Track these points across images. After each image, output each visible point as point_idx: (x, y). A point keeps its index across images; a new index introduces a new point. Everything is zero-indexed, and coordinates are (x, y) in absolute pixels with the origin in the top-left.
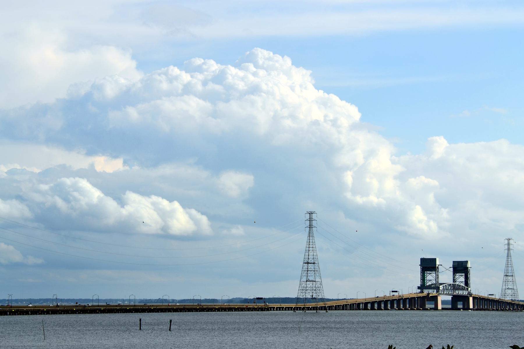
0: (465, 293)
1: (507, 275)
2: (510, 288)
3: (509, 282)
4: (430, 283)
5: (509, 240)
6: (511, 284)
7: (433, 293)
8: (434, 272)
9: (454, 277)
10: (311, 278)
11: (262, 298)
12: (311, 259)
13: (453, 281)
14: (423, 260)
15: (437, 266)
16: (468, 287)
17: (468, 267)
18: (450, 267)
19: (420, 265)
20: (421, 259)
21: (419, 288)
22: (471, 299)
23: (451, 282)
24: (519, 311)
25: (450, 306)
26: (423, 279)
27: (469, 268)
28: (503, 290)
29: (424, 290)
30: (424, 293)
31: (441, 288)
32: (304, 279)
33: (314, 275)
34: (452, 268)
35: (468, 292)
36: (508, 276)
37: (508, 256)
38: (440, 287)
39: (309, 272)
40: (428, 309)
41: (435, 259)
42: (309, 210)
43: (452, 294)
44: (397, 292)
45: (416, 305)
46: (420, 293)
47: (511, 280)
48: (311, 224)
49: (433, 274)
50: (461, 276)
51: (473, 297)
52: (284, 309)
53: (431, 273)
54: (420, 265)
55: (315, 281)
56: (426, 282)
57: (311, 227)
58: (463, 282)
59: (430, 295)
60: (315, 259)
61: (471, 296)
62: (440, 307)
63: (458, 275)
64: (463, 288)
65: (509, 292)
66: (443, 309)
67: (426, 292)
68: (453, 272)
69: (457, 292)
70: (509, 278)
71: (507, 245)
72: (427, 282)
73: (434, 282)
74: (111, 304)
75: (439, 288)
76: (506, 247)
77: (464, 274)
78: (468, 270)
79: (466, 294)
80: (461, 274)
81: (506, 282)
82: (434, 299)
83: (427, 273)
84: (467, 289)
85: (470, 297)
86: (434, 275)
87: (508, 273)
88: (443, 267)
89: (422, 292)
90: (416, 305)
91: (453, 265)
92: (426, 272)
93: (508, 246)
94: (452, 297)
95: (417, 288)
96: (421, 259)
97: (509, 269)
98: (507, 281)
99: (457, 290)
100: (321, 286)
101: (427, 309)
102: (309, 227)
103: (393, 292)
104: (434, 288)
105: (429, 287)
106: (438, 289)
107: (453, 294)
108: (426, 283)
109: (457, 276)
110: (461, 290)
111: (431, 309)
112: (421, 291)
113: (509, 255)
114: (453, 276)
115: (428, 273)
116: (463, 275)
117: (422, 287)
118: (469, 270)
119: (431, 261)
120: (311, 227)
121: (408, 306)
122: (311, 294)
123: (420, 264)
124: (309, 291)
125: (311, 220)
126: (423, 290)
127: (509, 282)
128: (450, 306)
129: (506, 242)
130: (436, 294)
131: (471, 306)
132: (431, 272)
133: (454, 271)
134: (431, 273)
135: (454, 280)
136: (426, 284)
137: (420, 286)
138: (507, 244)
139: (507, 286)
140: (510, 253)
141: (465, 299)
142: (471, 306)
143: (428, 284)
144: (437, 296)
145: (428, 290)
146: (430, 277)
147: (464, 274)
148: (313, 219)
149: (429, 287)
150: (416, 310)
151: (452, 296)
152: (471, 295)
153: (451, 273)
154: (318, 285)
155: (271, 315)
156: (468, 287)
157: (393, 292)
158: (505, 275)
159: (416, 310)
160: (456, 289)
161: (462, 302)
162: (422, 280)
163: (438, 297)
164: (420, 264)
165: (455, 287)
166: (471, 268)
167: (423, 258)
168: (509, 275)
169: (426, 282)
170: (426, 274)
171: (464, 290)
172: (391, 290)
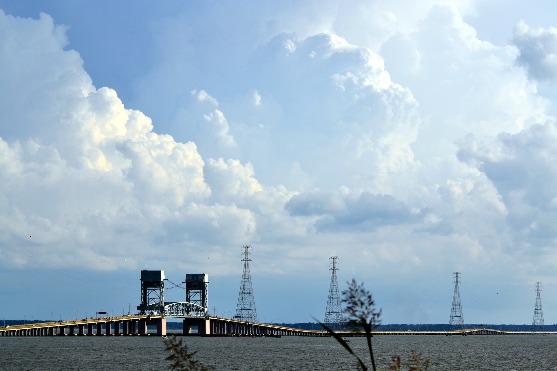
0: (200, 315)
1: (332, 297)
2: (334, 311)
3: (334, 305)
6: (248, 303)
7: (156, 314)
8: (158, 289)
9: (187, 295)
13: (187, 300)
15: (162, 280)
16: (204, 307)
17: (205, 282)
18: (183, 282)
19: (140, 279)
20: (142, 271)
21: (138, 308)
22: (208, 323)
24: (268, 337)
27: (206, 284)
28: (327, 314)
29: (145, 311)
30: (145, 314)
31: (166, 308)
34: (185, 283)
36: (332, 298)
38: (165, 307)
40: (103, 335)
41: (160, 272)
42: (333, 255)
43: (182, 316)
44: (104, 313)
45: (128, 330)
46: (140, 314)
47: (248, 299)
48: (247, 258)
50: (196, 293)
51: (210, 319)
52: (312, 334)
53: (154, 290)
54: (140, 279)
56: (148, 301)
57: (246, 260)
58: (198, 301)
59: (151, 318)
61: (208, 319)
62: (164, 332)
64: (197, 309)
65: (457, 319)
66: (168, 335)
67: (147, 313)
68: (186, 289)
70: (334, 300)
71: (332, 270)
75: (163, 308)
77: (201, 291)
78: (204, 286)
79: (202, 316)
81: (243, 300)
82: (157, 323)
83: (149, 290)
84: (203, 310)
85: (206, 320)
86: (158, 292)
87: (245, 289)
88: (169, 282)
89: (142, 313)
90: (128, 330)
91: (186, 281)
92: (148, 288)
93: (333, 265)
94: (184, 320)
95: (136, 308)
96: (142, 271)
97: (246, 285)
98: (243, 299)
99: (195, 311)
101: (147, 335)
102: (333, 269)
103: (100, 313)
104: (156, 309)
105: (153, 308)
106: (161, 309)
107: (197, 316)
108: (148, 302)
109: (191, 294)
110: (194, 311)
111: (152, 335)
112: (141, 312)
113: (334, 275)
114: (186, 293)
116: (198, 293)
117: (143, 308)
118: (206, 286)
119: (145, 274)
120: (246, 260)
121: (137, 331)
123: (141, 278)
126: (144, 311)
128: (181, 331)
129: (455, 275)
130: (160, 316)
131: (208, 331)
132: (153, 288)
134: (154, 290)
135: (188, 299)
137: (140, 306)
138: (333, 263)
139: (331, 309)
140: (458, 285)
141: (200, 323)
142: (208, 331)
144: (161, 318)
145: (151, 311)
146: (153, 295)
147: (201, 291)
148: (336, 263)
149: (153, 308)
150: (122, 336)
151: (184, 319)
152: (207, 317)
155: (424, 337)
157: (100, 313)
158: (242, 292)
159: (122, 336)
160: (189, 310)
161: (197, 327)
162: (142, 299)
165: (188, 308)
166: (208, 283)
167: (144, 270)
168: (334, 297)
169: (148, 301)
170: (148, 291)
171: (199, 311)
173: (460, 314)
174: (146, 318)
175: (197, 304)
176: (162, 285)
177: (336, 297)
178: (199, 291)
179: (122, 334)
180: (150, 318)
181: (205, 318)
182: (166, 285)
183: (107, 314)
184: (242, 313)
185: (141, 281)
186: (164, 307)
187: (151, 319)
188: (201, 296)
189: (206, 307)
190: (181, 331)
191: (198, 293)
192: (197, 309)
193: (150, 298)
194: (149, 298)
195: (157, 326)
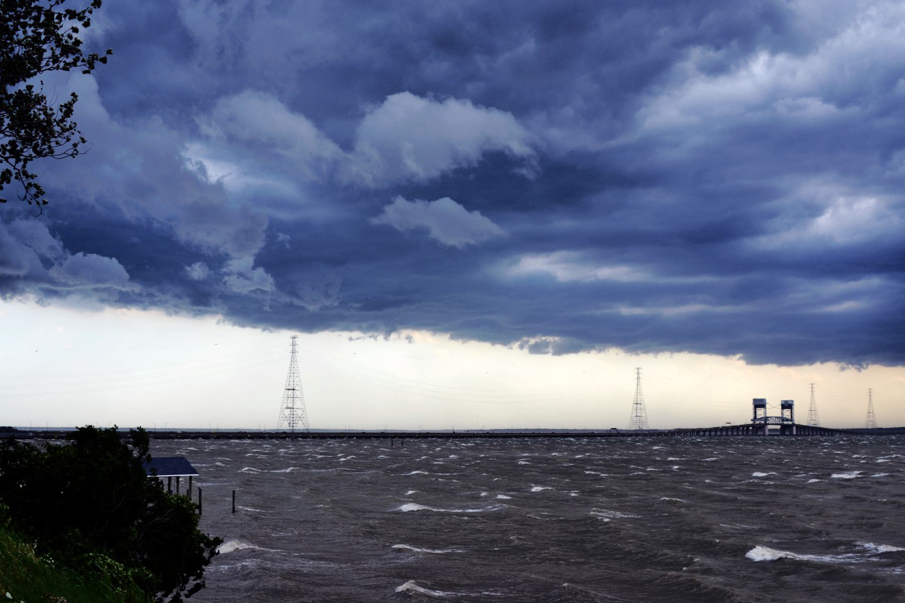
0: (790, 423)
5: (812, 384)
10: (639, 415)
11: (615, 429)
14: (755, 400)
21: (752, 420)
22: (794, 428)
23: (780, 416)
25: (779, 433)
32: (635, 415)
37: (637, 385)
39: (295, 399)
49: (762, 409)
63: (785, 410)
69: (785, 423)
73: (763, 416)
74: (556, 432)
76: (869, 394)
86: (763, 410)
103: (727, 423)
105: (761, 419)
109: (784, 411)
125: (870, 392)
129: (868, 391)
131: (795, 433)
135: (782, 414)
142: (795, 433)
146: (760, 412)
153: (780, 410)
154: (644, 419)
157: (727, 423)
165: (783, 419)
192: (787, 420)
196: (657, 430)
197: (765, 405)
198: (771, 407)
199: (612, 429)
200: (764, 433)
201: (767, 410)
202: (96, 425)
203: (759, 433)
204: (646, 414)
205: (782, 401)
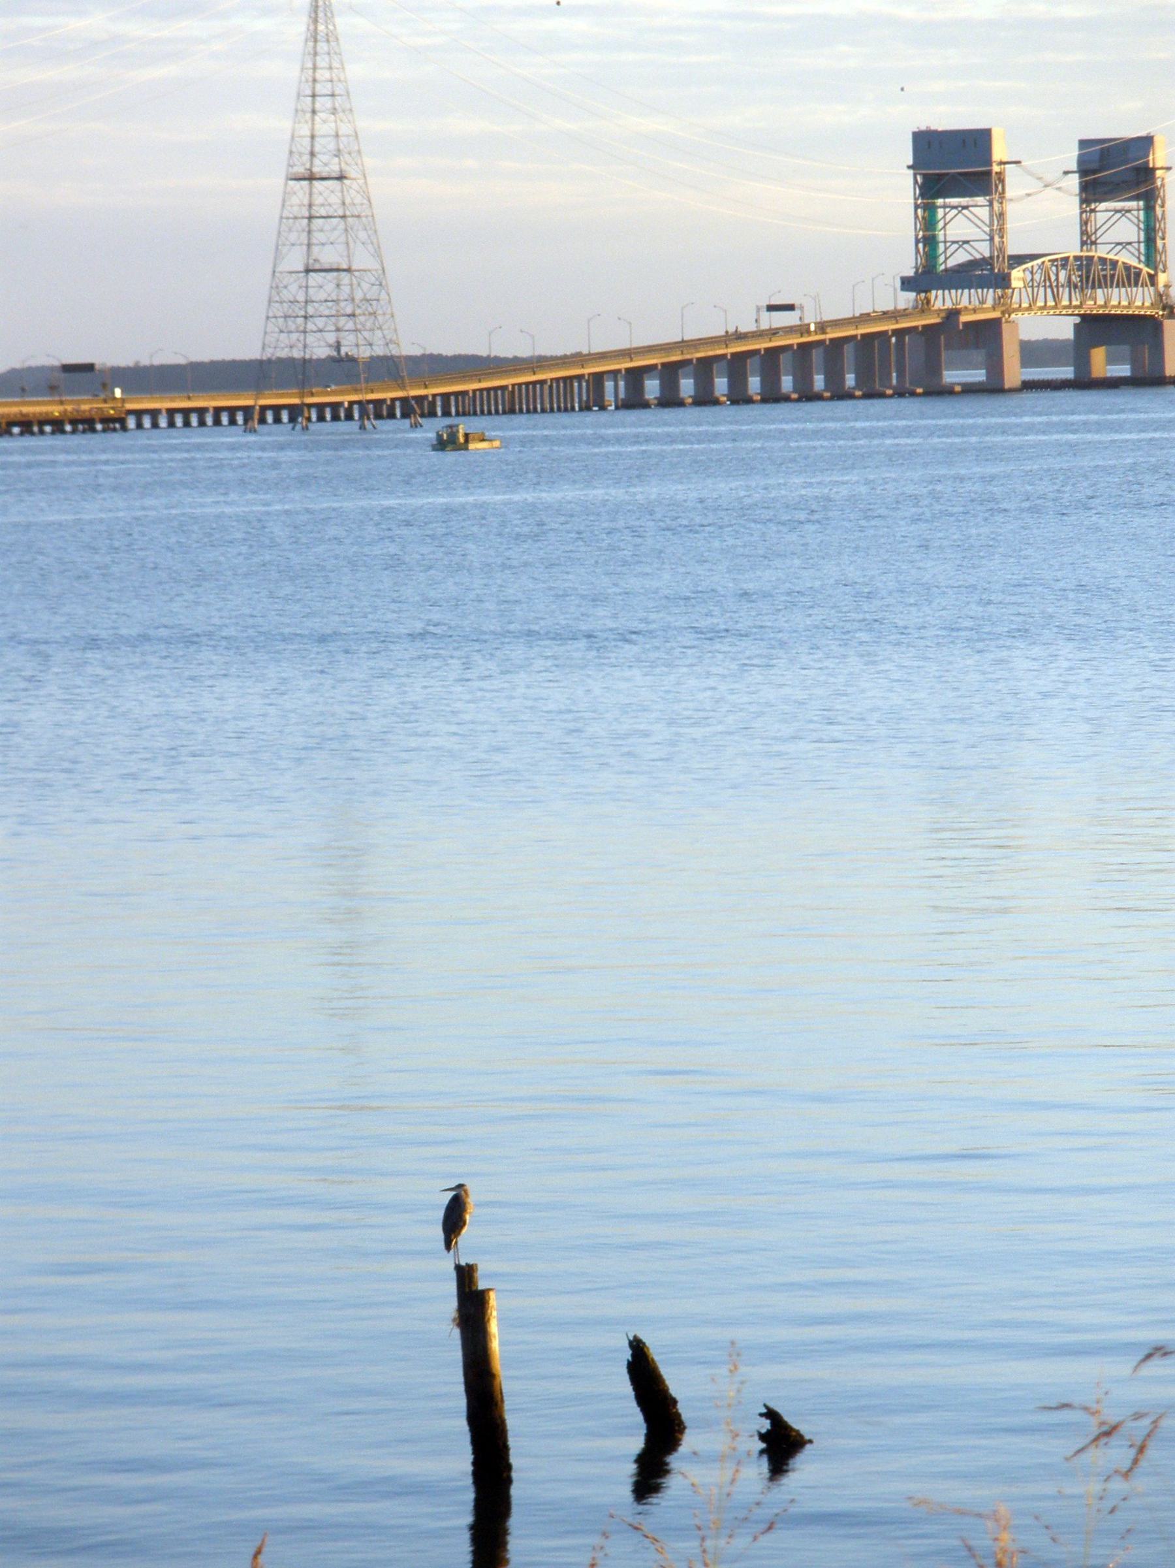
0: (1140, 300)
3: (321, 221)
4: (960, 257)
8: (980, 200)
9: (1084, 223)
10: (328, 256)
11: (90, 367)
12: (325, 158)
13: (1083, 243)
17: (1154, 169)
18: (1066, 173)
19: (909, 167)
23: (1072, 248)
26: (928, 240)
32: (295, 260)
33: (343, 239)
35: (1157, 291)
43: (1076, 307)
44: (790, 308)
45: (894, 375)
49: (979, 207)
50: (1119, 215)
53: (966, 207)
54: (909, 167)
55: (348, 270)
58: (1130, 243)
60: (346, 156)
72: (948, 253)
73: (984, 250)
77: (1141, 203)
80: (1119, 205)
83: (944, 207)
84: (1153, 279)
86: (984, 213)
92: (940, 201)
94: (1076, 325)
95: (898, 284)
99: (1124, 286)
100: (383, 295)
103: (771, 308)
105: (965, 276)
109: (1101, 217)
111: (970, 390)
115: (955, 207)
116: (1129, 211)
122: (331, 338)
124: (320, 322)
127: (317, 223)
132: (964, 201)
133: (1084, 187)
134: (966, 207)
135: (1088, 239)
136: (945, 262)
143: (951, 263)
147: (1141, 203)
149: (965, 276)
151: (1078, 320)
156: (1156, 269)
157: (771, 308)
162: (921, 246)
163: (1004, 326)
164: (911, 163)
167: (923, 128)
169: (945, 252)
170: (940, 212)
171: (1136, 285)
172: (765, 303)
173: (341, 248)
174: (938, 320)
175: (1126, 258)
176: (997, 187)
177: (336, 168)
178: (1133, 204)
179: (724, 395)
180: (958, 319)
181: (1161, 313)
182: (1015, 184)
183: (802, 311)
184: (311, 291)
185: (915, 176)
186: (1009, 275)
187: (966, 324)
188: (1142, 226)
189: (1161, 267)
190: (1066, 372)
191: (1129, 211)
192: (1131, 277)
193: (953, 242)
194: (945, 242)
195: (983, 351)
196: (1058, 340)
197: (1001, 177)
198: (970, 209)
199: (68, 369)
200: (995, 366)
201: (1011, 209)
202: (444, 354)
203: (952, 376)
204: (378, 254)
205: (1083, 143)
